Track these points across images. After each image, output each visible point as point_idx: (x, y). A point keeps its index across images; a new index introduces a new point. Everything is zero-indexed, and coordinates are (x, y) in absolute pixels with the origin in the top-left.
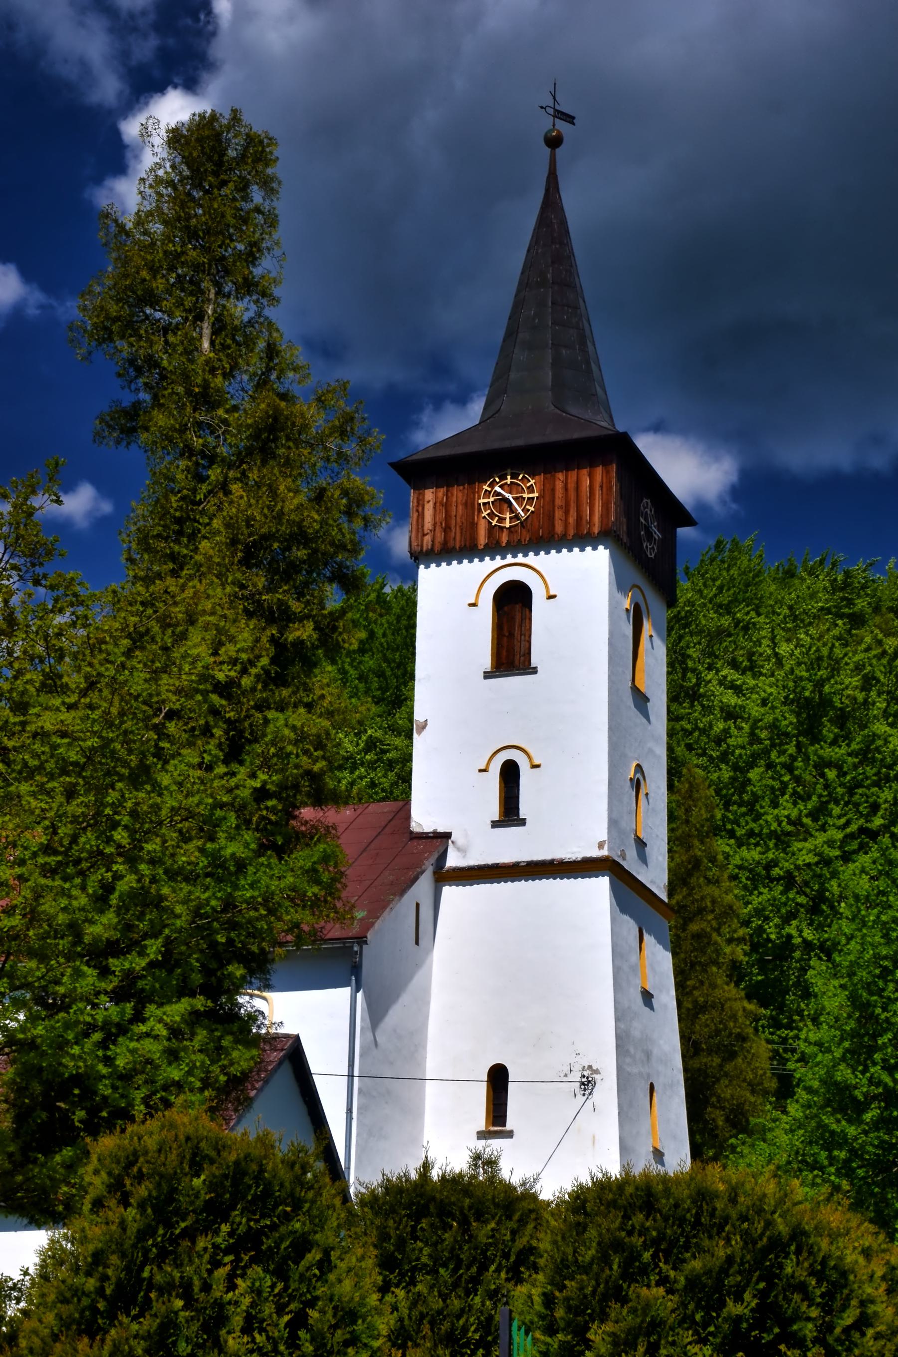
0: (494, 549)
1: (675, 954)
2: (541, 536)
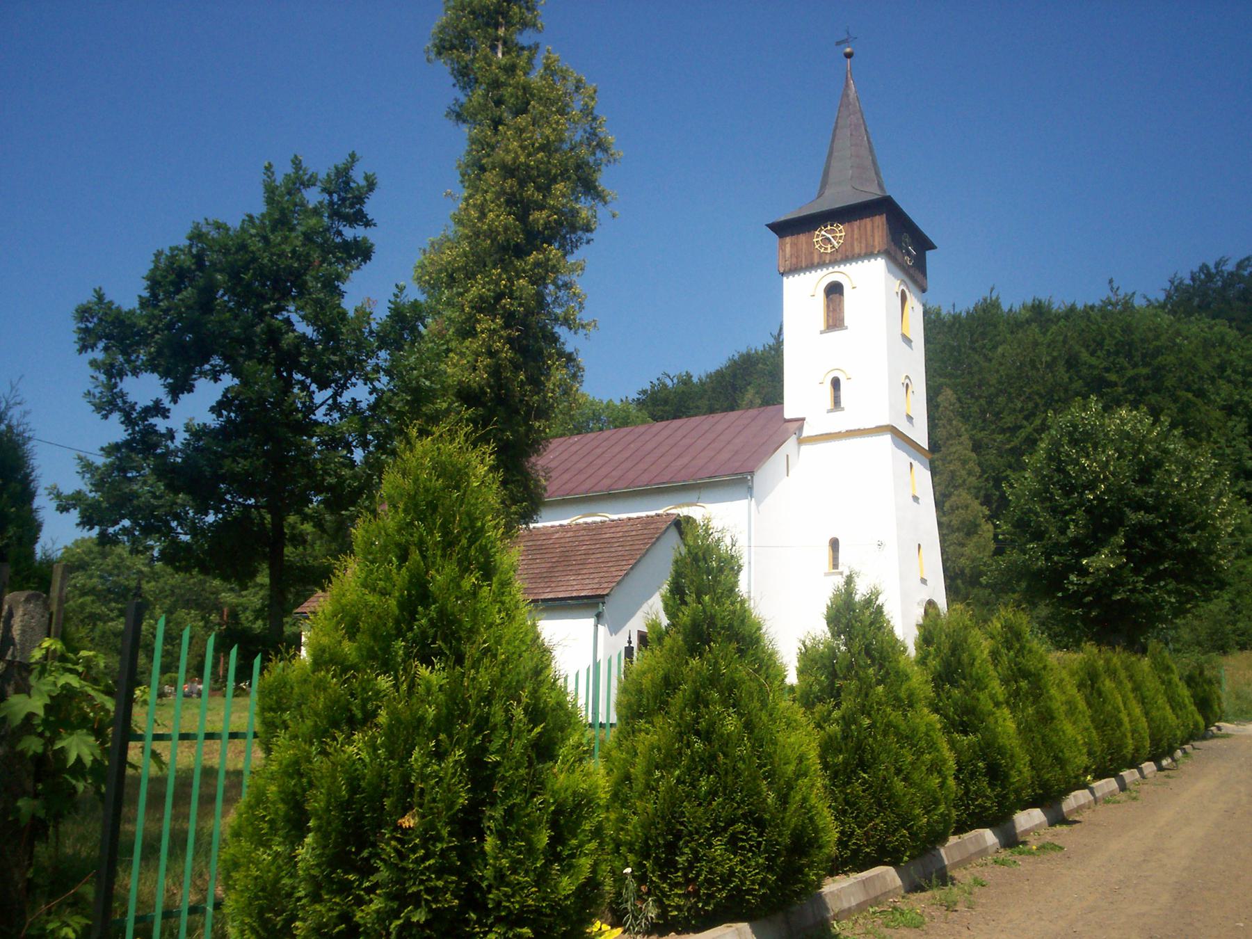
0: (822, 264)
1: (934, 473)
2: (846, 256)
